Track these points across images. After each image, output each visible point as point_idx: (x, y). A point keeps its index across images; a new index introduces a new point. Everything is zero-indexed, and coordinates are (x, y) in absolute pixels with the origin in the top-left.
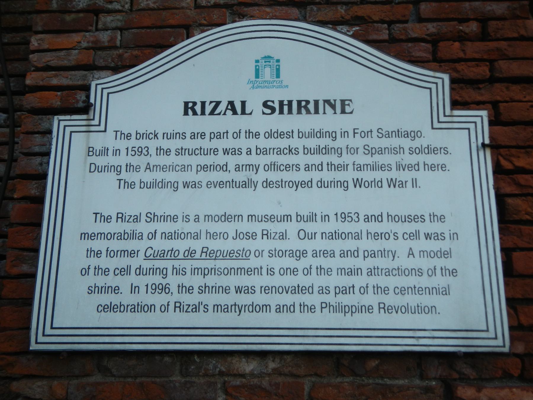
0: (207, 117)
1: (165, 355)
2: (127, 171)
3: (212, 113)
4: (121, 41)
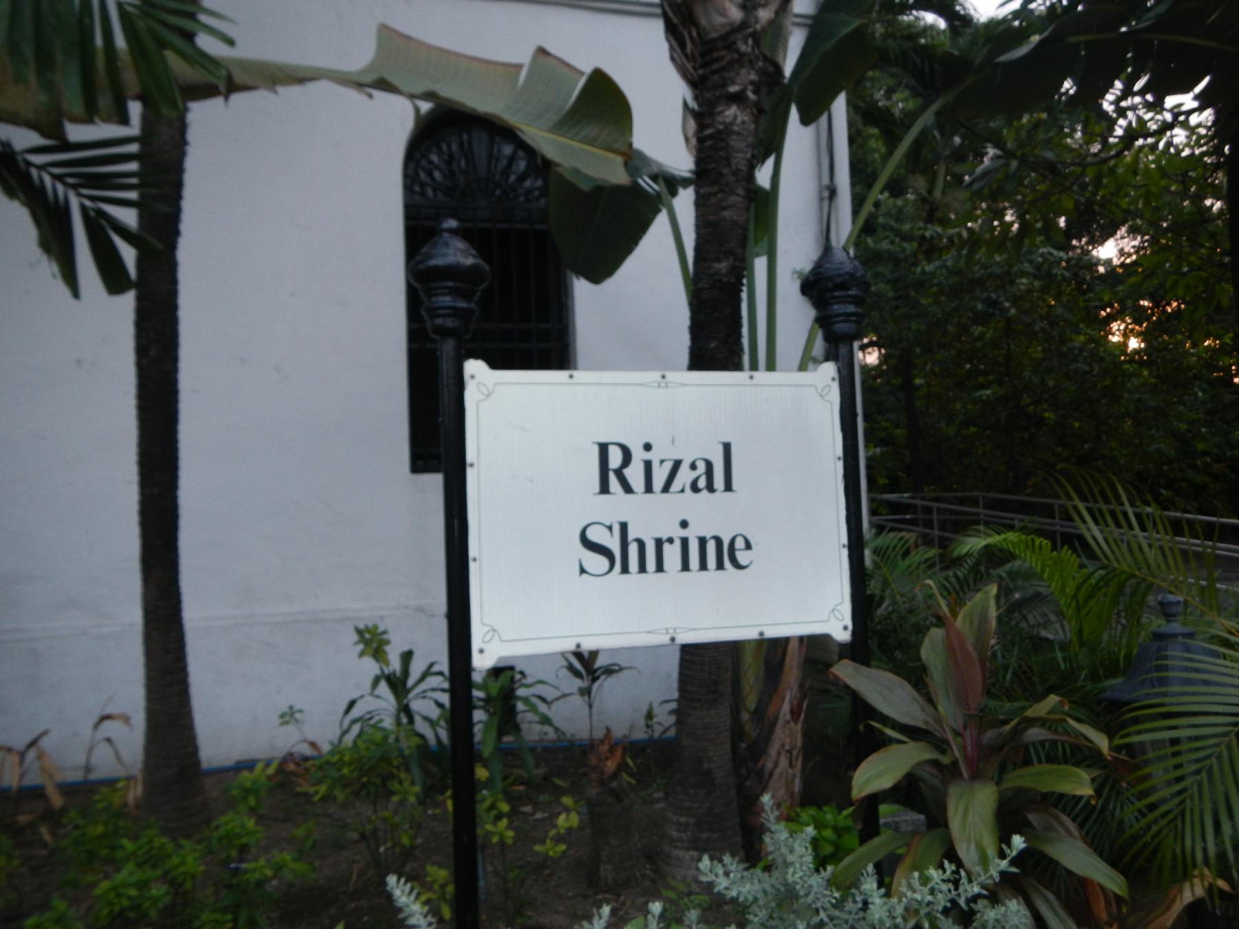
0: (657, 497)
3: (666, 488)
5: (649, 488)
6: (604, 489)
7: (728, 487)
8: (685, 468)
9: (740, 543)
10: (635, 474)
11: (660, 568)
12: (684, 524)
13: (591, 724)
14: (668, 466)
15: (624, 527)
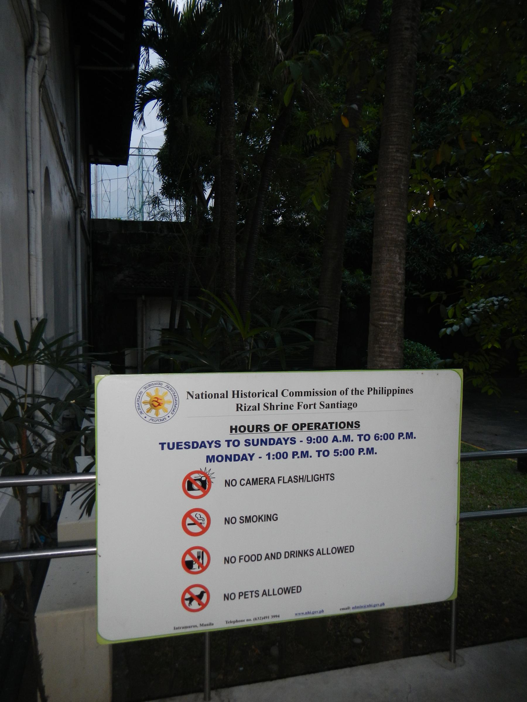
0: (246, 412)
1: (468, 223)
2: (352, 394)
3: (248, 410)
4: (461, 202)
6: (237, 410)
8: (252, 407)
10: (243, 408)
13: (10, 495)
14: (248, 407)
15: (271, 404)
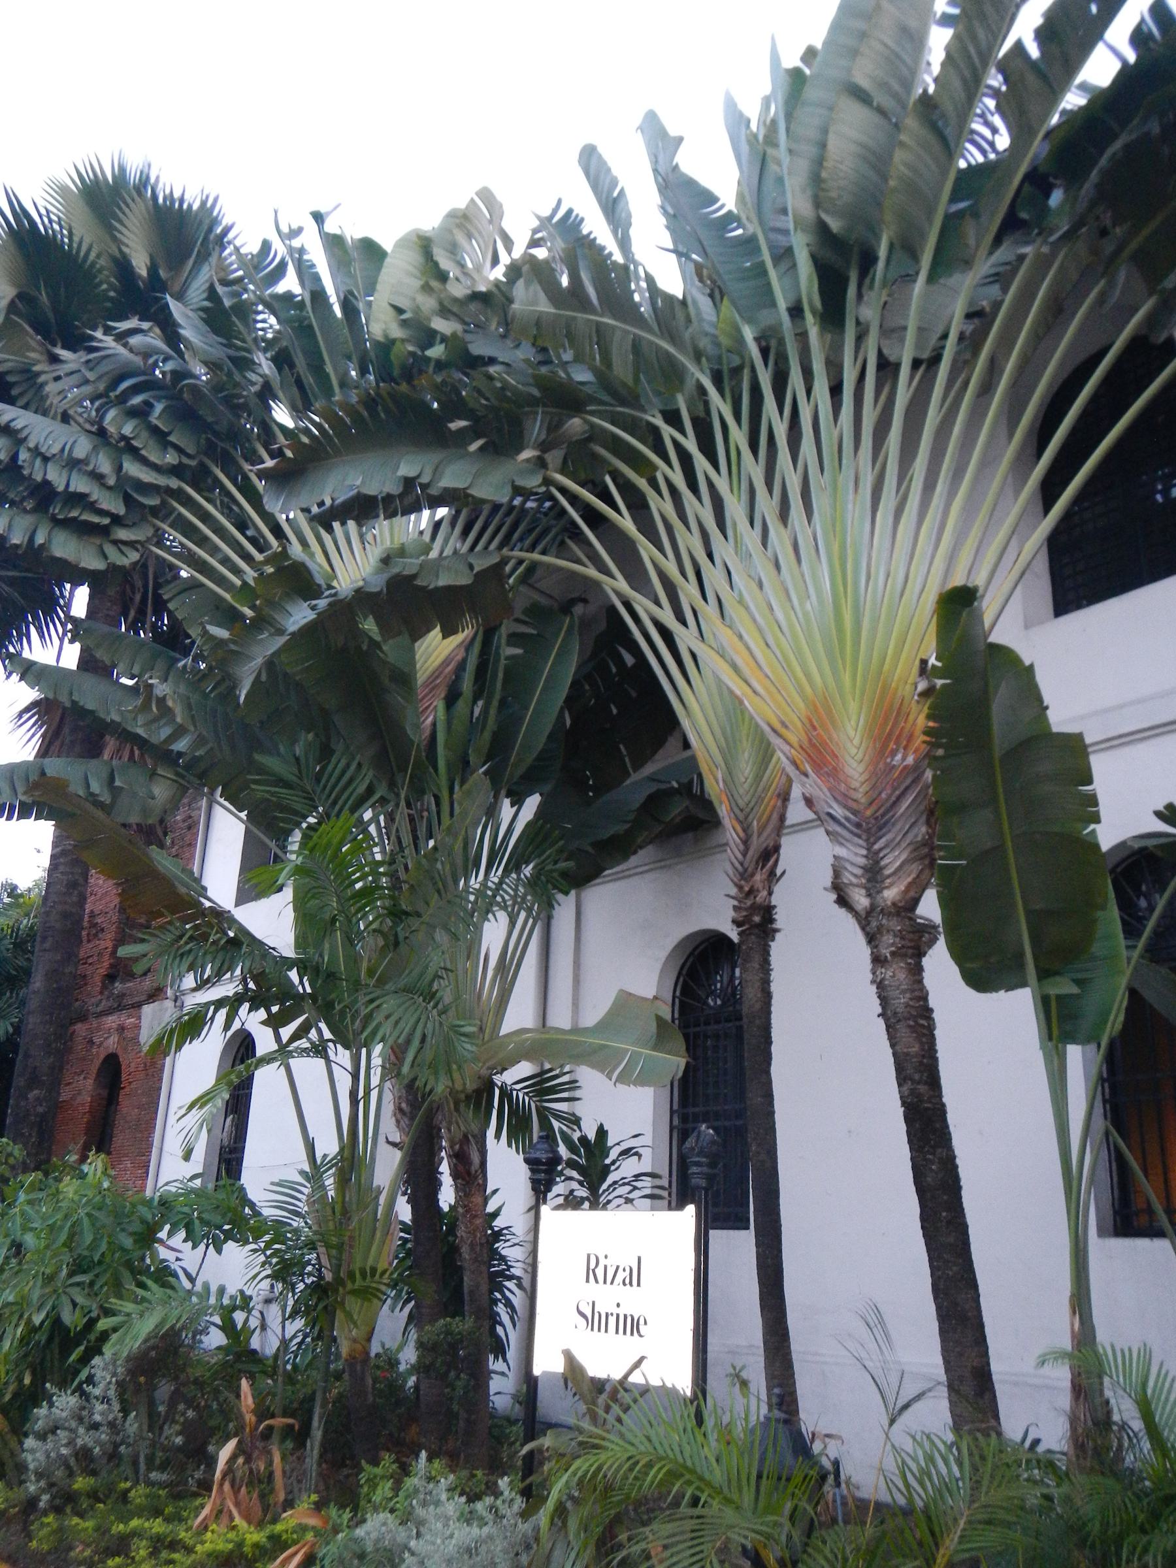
3: (612, 1283)
5: (605, 1282)
7: (639, 1285)
8: (621, 1270)
9: (642, 1321)
11: (606, 1331)
12: (618, 1305)
15: (594, 1303)
